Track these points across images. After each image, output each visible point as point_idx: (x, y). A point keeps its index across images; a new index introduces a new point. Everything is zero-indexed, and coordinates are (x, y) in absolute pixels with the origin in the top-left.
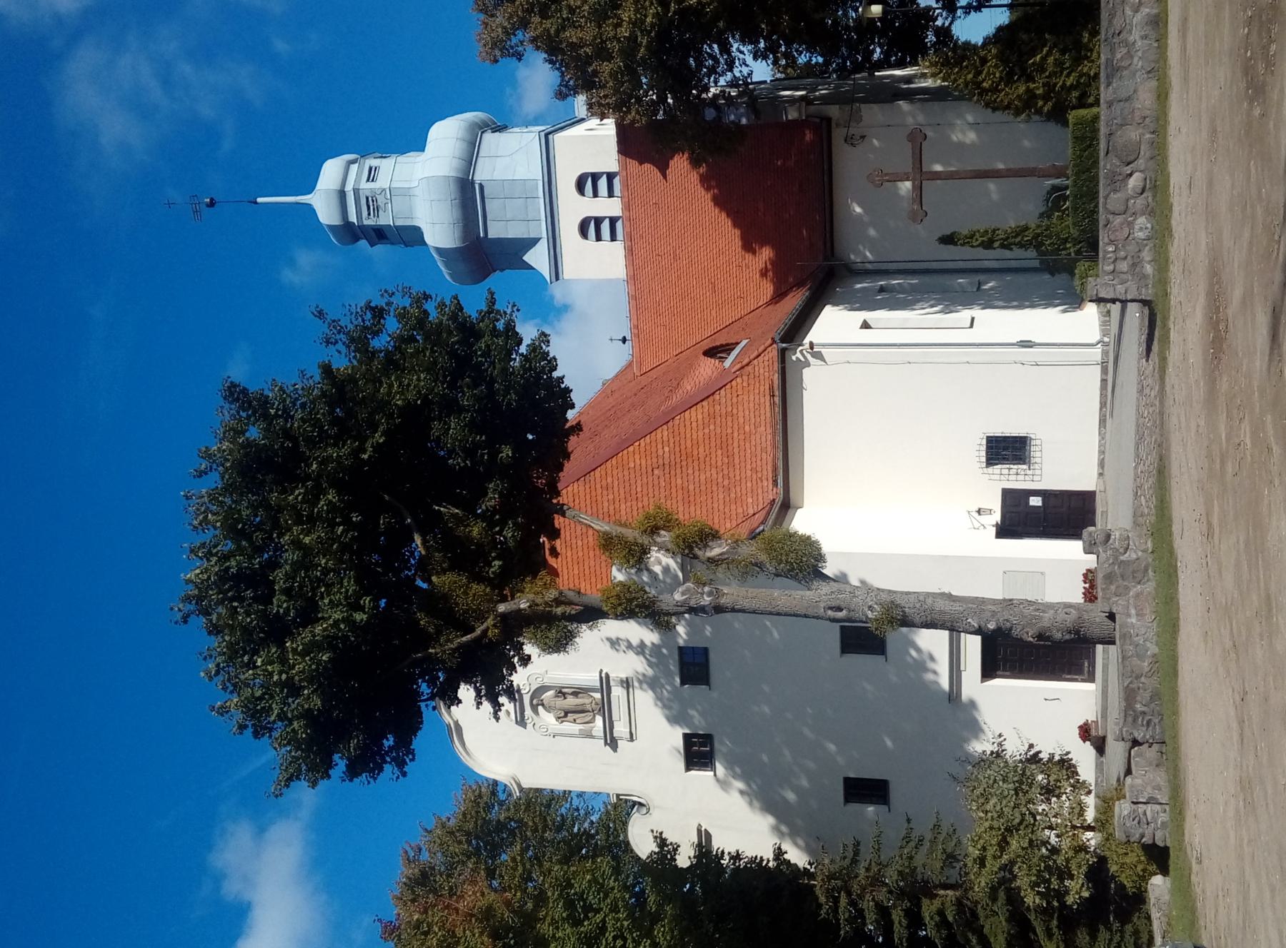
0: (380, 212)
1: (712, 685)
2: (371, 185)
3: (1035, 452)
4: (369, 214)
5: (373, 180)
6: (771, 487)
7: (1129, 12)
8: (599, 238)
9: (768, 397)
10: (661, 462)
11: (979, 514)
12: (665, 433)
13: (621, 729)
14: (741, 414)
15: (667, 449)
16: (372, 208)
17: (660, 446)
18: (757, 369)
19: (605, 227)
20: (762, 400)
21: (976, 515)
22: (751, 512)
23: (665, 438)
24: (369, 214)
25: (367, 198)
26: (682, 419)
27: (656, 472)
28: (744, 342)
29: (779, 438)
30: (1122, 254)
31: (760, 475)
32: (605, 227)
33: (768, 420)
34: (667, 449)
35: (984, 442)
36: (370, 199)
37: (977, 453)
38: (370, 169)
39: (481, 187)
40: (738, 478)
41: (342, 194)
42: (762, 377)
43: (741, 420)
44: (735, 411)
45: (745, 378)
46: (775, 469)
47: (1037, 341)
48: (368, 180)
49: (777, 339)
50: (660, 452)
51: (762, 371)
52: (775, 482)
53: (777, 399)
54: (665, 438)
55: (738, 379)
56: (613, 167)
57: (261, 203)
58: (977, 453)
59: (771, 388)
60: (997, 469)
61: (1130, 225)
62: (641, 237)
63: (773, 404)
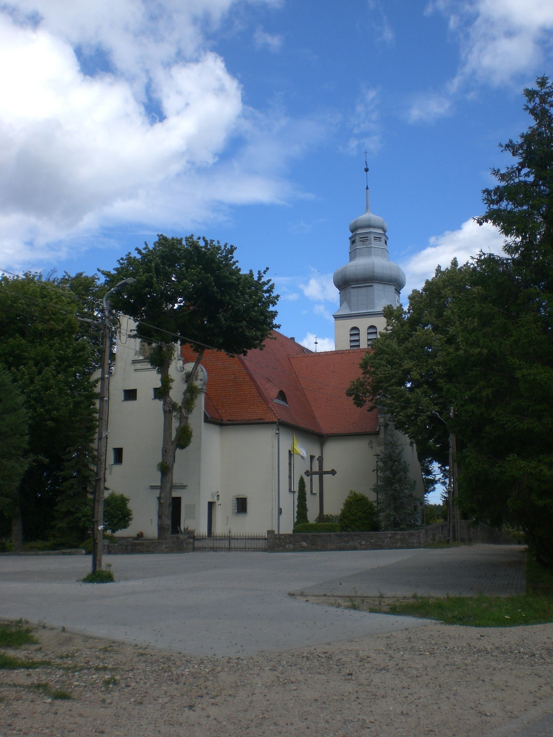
0: (362, 243)
1: (154, 400)
2: (373, 239)
3: (241, 516)
4: (361, 238)
5: (375, 239)
6: (228, 419)
7: (358, 541)
8: (351, 335)
9: (259, 418)
10: (237, 377)
11: (217, 496)
12: (247, 379)
13: (139, 366)
14: (254, 407)
15: (241, 379)
16: (364, 239)
17: (242, 377)
18: (270, 413)
19: (356, 338)
20: (258, 415)
21: (217, 494)
22: (219, 411)
23: (246, 379)
24: (361, 238)
25: (367, 237)
26: (252, 385)
27: (233, 376)
28: (287, 405)
29: (245, 422)
30: (281, 541)
31: (232, 415)
32: (356, 338)
33: (251, 418)
34: (241, 379)
35: (244, 497)
36: (367, 238)
37: (242, 495)
38: (380, 238)
39: (372, 286)
40: (231, 406)
41: (369, 226)
42: (267, 415)
43: (252, 408)
44: (255, 405)
45: (267, 409)
46: (234, 420)
47: (280, 517)
48: (375, 237)
49: (280, 421)
50: (240, 377)
51: (269, 415)
52: (229, 420)
53: (258, 421)
54: (246, 379)
55: (266, 406)
56: (361, 347)
57: (100, 407)
58: (242, 495)
59: (262, 419)
60: (235, 502)
61: (291, 543)
62: (342, 358)
63: (257, 419)
